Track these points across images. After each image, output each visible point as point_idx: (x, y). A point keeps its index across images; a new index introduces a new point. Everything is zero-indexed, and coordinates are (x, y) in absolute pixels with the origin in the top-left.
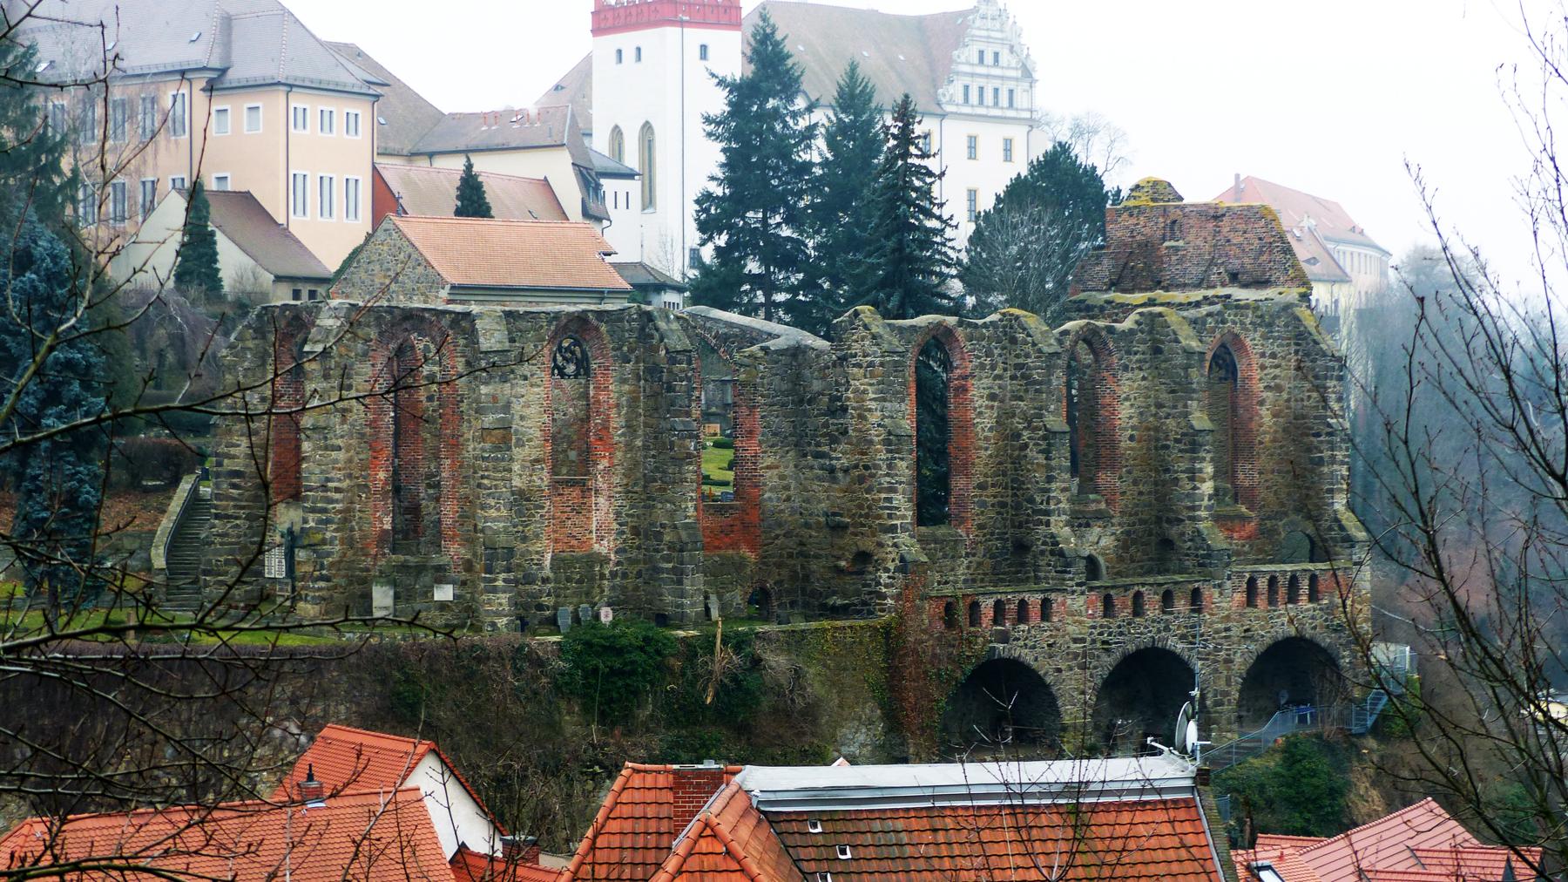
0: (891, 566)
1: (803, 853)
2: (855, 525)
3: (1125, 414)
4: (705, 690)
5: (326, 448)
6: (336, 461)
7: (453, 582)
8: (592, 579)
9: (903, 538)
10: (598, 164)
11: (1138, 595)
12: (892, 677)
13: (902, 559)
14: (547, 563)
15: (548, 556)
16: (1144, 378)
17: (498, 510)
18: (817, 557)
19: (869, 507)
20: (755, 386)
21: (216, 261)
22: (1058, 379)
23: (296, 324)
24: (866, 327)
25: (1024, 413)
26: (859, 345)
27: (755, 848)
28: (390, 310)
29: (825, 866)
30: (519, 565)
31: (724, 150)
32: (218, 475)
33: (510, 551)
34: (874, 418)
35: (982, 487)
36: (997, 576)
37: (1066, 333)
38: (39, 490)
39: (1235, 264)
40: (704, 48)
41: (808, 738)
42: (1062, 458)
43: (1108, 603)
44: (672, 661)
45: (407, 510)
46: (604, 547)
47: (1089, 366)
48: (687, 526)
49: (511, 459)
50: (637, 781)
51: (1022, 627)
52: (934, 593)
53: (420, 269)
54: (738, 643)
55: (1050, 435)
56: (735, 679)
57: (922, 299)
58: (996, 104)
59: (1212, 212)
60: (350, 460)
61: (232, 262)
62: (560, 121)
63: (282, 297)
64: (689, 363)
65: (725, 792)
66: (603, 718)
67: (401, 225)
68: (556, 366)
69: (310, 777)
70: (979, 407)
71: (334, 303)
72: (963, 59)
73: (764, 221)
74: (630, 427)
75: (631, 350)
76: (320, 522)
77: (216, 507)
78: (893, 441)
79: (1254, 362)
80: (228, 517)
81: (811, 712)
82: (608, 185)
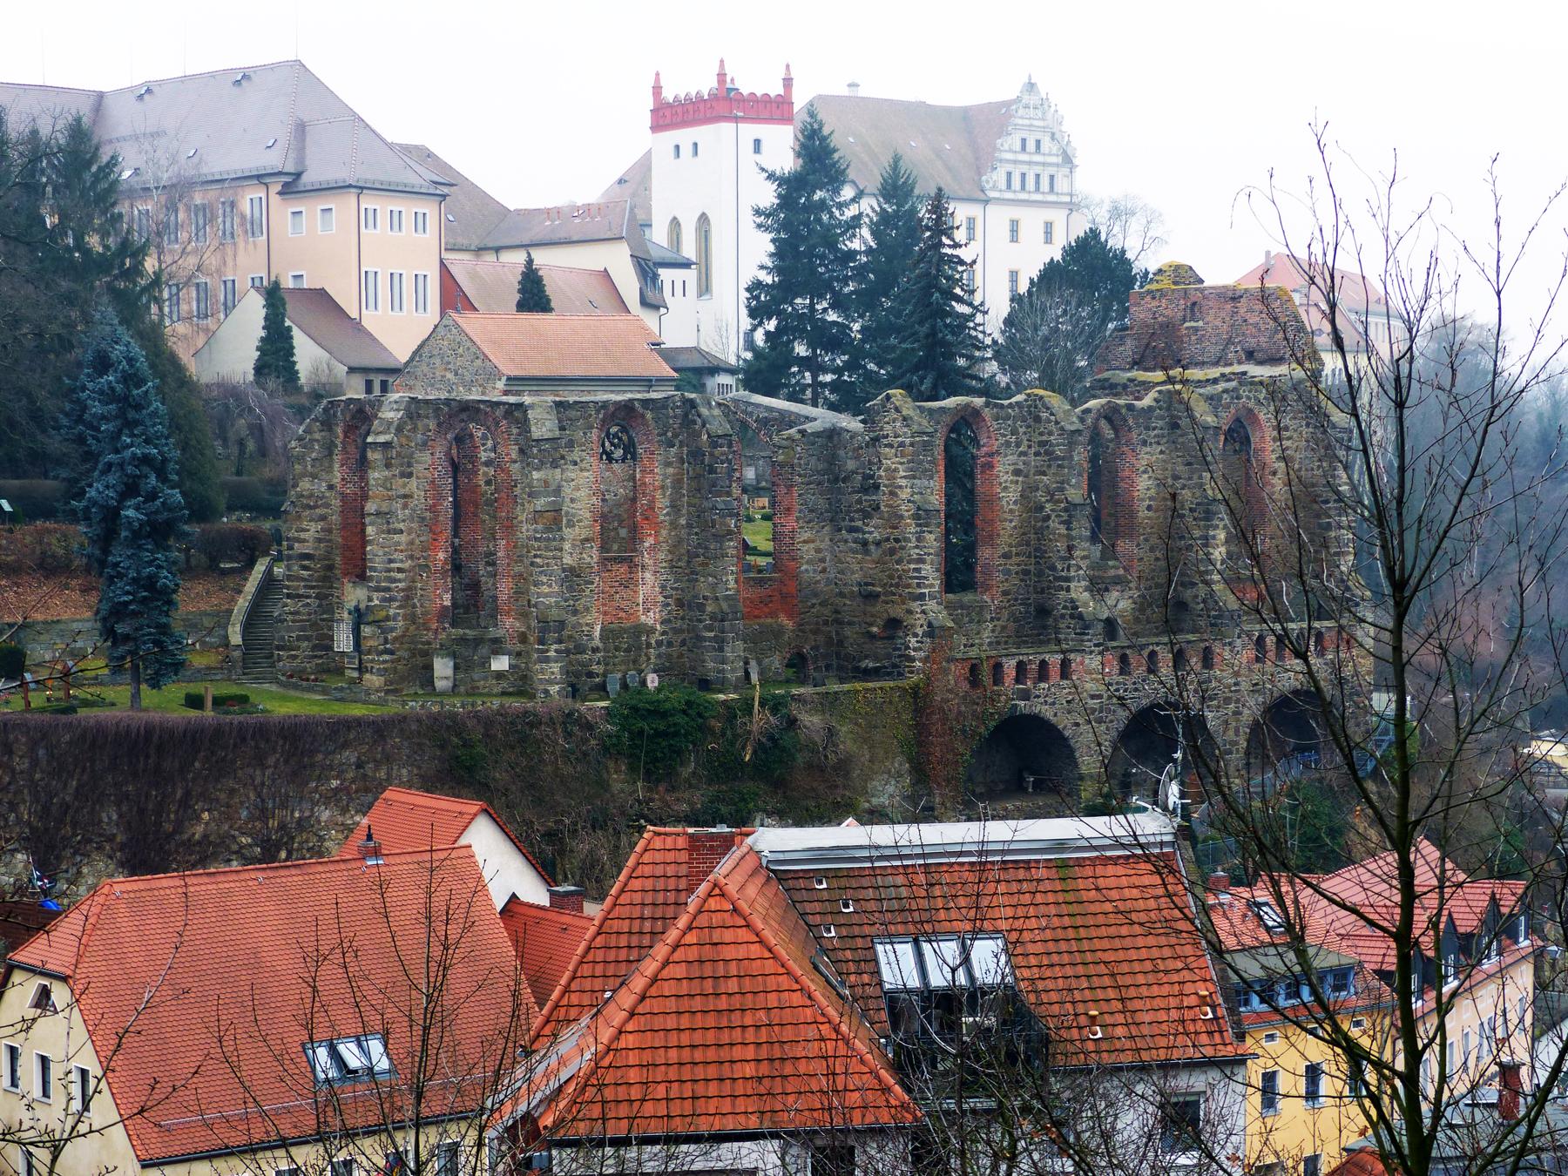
0: (920, 631)
1: (809, 908)
2: (885, 594)
3: (1144, 486)
4: (744, 748)
5: (389, 532)
6: (399, 543)
7: (509, 654)
8: (640, 649)
9: (931, 605)
10: (656, 254)
11: (1153, 654)
12: (920, 734)
13: (930, 625)
14: (597, 634)
15: (598, 628)
16: (1162, 452)
17: (550, 586)
18: (850, 623)
19: (900, 577)
20: (792, 466)
21: (292, 355)
22: (1081, 455)
23: (361, 416)
24: (897, 410)
25: (1047, 486)
26: (891, 427)
27: (762, 904)
28: (448, 402)
29: (829, 918)
30: (570, 637)
31: (773, 241)
32: (289, 558)
33: (562, 624)
34: (904, 494)
35: (1006, 556)
36: (1021, 639)
37: (1088, 411)
38: (120, 576)
39: (1252, 343)
40: (757, 142)
41: (840, 791)
42: (1082, 528)
43: (1124, 660)
44: (713, 722)
45: (468, 587)
46: (650, 618)
47: (1111, 441)
48: (727, 598)
49: (562, 539)
50: (658, 843)
51: (1042, 685)
52: (959, 656)
53: (478, 362)
54: (775, 705)
55: (1071, 507)
56: (771, 738)
57: (951, 382)
58: (1037, 189)
59: (1230, 294)
60: (412, 543)
61: (308, 355)
62: (623, 217)
63: (355, 390)
64: (730, 446)
65: (736, 853)
66: (648, 775)
67: (460, 321)
68: (605, 451)
69: (369, 837)
70: (1004, 482)
71: (395, 396)
72: (1006, 147)
73: (812, 306)
74: (675, 507)
75: (676, 436)
76: (384, 600)
77: (288, 587)
78: (922, 515)
79: (1267, 434)
80: (300, 596)
81: (843, 767)
82: (665, 274)
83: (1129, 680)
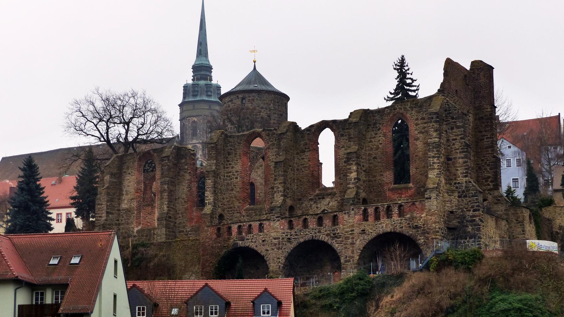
8: (151, 235)
83: (293, 232)
